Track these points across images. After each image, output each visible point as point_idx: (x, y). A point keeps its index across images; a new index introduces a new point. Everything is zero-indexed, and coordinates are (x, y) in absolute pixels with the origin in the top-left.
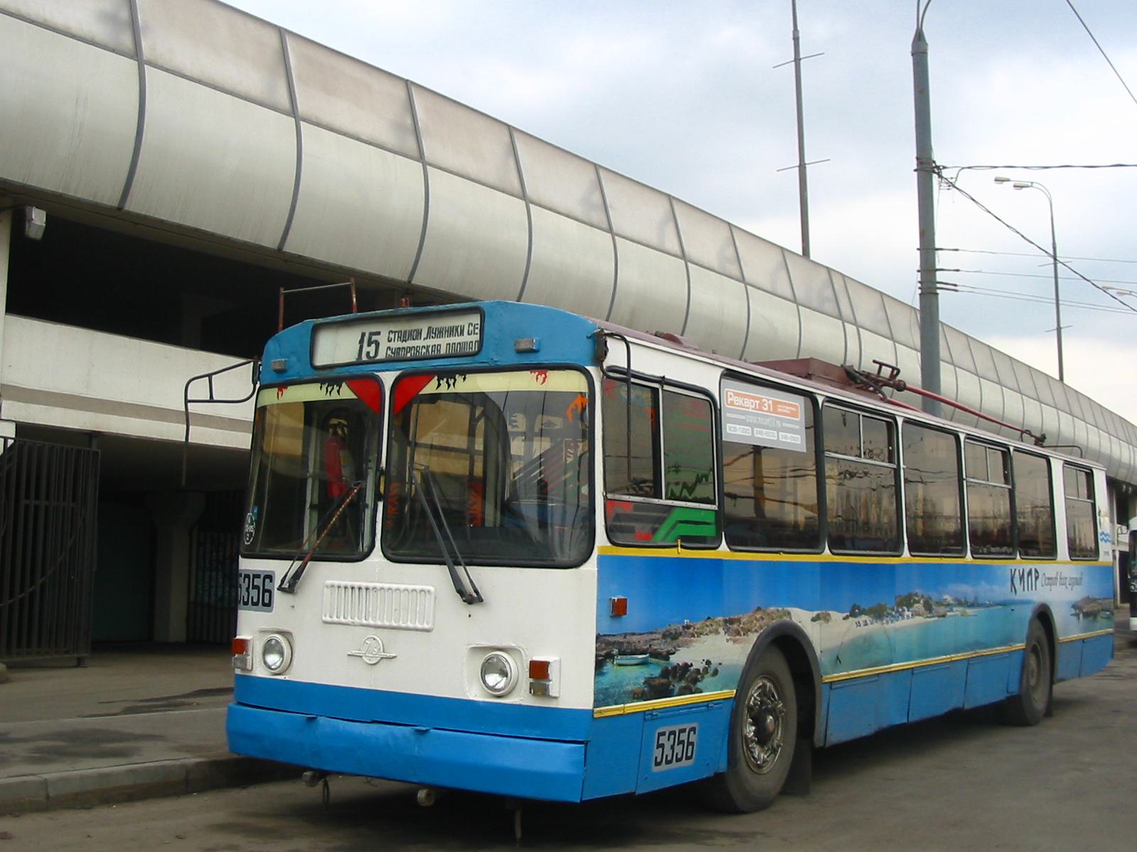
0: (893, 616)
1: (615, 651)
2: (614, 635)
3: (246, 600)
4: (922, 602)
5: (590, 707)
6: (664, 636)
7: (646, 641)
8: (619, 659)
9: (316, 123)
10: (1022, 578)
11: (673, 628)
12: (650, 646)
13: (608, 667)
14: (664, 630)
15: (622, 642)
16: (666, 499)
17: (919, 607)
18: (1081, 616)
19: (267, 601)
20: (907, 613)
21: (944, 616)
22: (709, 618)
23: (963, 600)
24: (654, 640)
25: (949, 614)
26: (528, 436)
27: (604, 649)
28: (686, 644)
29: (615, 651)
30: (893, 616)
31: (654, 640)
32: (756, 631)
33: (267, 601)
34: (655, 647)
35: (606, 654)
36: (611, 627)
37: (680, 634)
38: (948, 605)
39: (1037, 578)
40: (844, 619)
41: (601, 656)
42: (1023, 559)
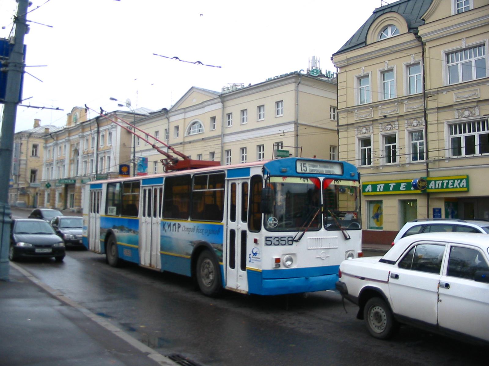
17: (132, 232)
39: (179, 227)
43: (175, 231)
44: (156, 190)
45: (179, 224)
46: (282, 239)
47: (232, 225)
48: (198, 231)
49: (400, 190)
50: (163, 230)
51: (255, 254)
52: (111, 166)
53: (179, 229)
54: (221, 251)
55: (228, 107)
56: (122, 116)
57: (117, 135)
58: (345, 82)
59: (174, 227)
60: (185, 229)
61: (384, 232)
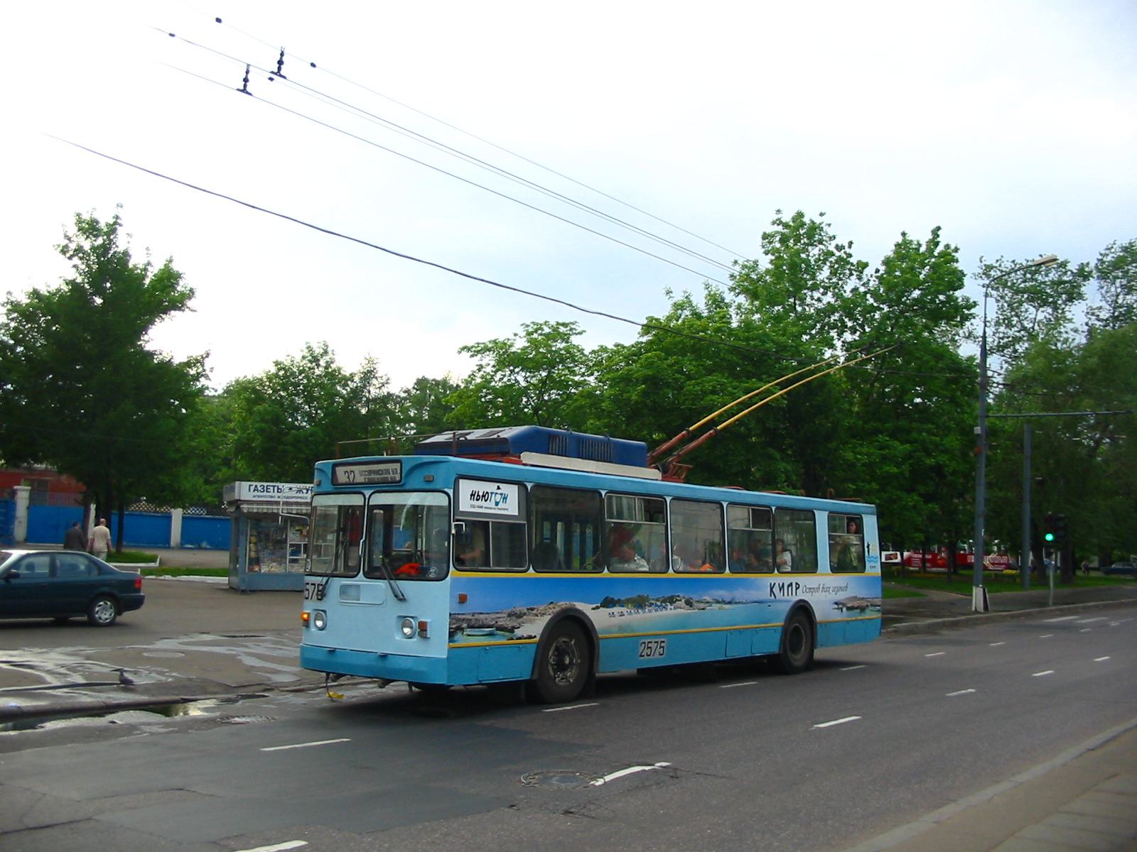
0: (656, 605)
1: (465, 625)
2: (463, 614)
4: (683, 600)
6: (509, 615)
7: (493, 619)
8: (468, 631)
9: (187, 569)
11: (517, 610)
12: (497, 622)
13: (458, 636)
14: (509, 611)
15: (471, 620)
16: (488, 522)
17: (682, 603)
18: (844, 609)
20: (669, 606)
21: (703, 609)
22: (552, 603)
23: (721, 600)
24: (500, 618)
25: (708, 608)
27: (454, 624)
28: (531, 621)
29: (465, 625)
30: (656, 605)
31: (500, 618)
32: (550, 614)
34: (501, 623)
35: (457, 627)
36: (458, 609)
37: (525, 614)
38: (708, 602)
39: (797, 589)
40: (593, 609)
41: (452, 628)
43: (792, 594)
45: (797, 584)
50: (714, 599)
53: (798, 591)
59: (790, 588)
60: (806, 590)
61: (46, 732)
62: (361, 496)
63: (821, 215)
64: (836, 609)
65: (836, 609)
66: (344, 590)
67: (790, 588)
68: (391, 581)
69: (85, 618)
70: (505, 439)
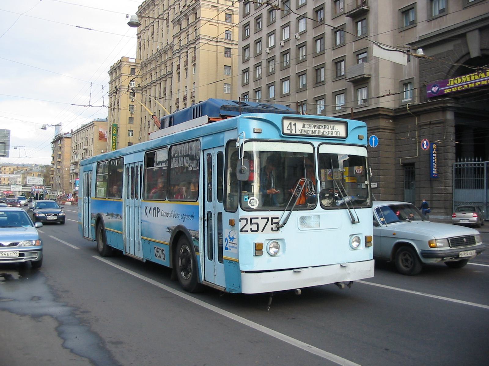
3: (159, 256)
5: (27, 177)
10: (150, 210)
19: (336, 132)
26: (48, 180)
33: (336, 132)
39: (158, 212)
42: (169, 201)
44: (137, 167)
46: (254, 221)
47: (209, 207)
48: (176, 216)
49: (315, 114)
51: (232, 239)
52: (291, 59)
53: (159, 213)
54: (198, 239)
55: (311, 54)
56: (47, 197)
57: (413, 26)
58: (217, 2)
59: (154, 211)
60: (163, 214)
62: (310, 145)
63: (127, 17)
64: (168, 231)
65: (168, 231)
66: (302, 220)
67: (154, 211)
68: (351, 210)
69: (477, 250)
70: (119, 172)
